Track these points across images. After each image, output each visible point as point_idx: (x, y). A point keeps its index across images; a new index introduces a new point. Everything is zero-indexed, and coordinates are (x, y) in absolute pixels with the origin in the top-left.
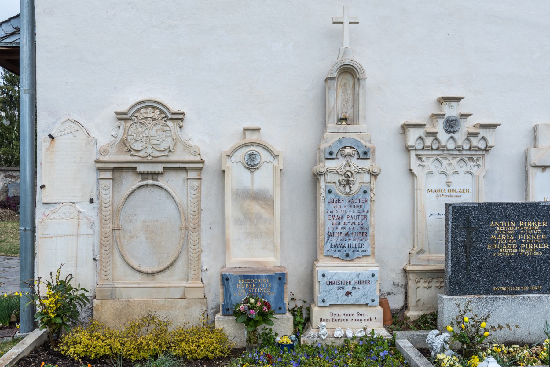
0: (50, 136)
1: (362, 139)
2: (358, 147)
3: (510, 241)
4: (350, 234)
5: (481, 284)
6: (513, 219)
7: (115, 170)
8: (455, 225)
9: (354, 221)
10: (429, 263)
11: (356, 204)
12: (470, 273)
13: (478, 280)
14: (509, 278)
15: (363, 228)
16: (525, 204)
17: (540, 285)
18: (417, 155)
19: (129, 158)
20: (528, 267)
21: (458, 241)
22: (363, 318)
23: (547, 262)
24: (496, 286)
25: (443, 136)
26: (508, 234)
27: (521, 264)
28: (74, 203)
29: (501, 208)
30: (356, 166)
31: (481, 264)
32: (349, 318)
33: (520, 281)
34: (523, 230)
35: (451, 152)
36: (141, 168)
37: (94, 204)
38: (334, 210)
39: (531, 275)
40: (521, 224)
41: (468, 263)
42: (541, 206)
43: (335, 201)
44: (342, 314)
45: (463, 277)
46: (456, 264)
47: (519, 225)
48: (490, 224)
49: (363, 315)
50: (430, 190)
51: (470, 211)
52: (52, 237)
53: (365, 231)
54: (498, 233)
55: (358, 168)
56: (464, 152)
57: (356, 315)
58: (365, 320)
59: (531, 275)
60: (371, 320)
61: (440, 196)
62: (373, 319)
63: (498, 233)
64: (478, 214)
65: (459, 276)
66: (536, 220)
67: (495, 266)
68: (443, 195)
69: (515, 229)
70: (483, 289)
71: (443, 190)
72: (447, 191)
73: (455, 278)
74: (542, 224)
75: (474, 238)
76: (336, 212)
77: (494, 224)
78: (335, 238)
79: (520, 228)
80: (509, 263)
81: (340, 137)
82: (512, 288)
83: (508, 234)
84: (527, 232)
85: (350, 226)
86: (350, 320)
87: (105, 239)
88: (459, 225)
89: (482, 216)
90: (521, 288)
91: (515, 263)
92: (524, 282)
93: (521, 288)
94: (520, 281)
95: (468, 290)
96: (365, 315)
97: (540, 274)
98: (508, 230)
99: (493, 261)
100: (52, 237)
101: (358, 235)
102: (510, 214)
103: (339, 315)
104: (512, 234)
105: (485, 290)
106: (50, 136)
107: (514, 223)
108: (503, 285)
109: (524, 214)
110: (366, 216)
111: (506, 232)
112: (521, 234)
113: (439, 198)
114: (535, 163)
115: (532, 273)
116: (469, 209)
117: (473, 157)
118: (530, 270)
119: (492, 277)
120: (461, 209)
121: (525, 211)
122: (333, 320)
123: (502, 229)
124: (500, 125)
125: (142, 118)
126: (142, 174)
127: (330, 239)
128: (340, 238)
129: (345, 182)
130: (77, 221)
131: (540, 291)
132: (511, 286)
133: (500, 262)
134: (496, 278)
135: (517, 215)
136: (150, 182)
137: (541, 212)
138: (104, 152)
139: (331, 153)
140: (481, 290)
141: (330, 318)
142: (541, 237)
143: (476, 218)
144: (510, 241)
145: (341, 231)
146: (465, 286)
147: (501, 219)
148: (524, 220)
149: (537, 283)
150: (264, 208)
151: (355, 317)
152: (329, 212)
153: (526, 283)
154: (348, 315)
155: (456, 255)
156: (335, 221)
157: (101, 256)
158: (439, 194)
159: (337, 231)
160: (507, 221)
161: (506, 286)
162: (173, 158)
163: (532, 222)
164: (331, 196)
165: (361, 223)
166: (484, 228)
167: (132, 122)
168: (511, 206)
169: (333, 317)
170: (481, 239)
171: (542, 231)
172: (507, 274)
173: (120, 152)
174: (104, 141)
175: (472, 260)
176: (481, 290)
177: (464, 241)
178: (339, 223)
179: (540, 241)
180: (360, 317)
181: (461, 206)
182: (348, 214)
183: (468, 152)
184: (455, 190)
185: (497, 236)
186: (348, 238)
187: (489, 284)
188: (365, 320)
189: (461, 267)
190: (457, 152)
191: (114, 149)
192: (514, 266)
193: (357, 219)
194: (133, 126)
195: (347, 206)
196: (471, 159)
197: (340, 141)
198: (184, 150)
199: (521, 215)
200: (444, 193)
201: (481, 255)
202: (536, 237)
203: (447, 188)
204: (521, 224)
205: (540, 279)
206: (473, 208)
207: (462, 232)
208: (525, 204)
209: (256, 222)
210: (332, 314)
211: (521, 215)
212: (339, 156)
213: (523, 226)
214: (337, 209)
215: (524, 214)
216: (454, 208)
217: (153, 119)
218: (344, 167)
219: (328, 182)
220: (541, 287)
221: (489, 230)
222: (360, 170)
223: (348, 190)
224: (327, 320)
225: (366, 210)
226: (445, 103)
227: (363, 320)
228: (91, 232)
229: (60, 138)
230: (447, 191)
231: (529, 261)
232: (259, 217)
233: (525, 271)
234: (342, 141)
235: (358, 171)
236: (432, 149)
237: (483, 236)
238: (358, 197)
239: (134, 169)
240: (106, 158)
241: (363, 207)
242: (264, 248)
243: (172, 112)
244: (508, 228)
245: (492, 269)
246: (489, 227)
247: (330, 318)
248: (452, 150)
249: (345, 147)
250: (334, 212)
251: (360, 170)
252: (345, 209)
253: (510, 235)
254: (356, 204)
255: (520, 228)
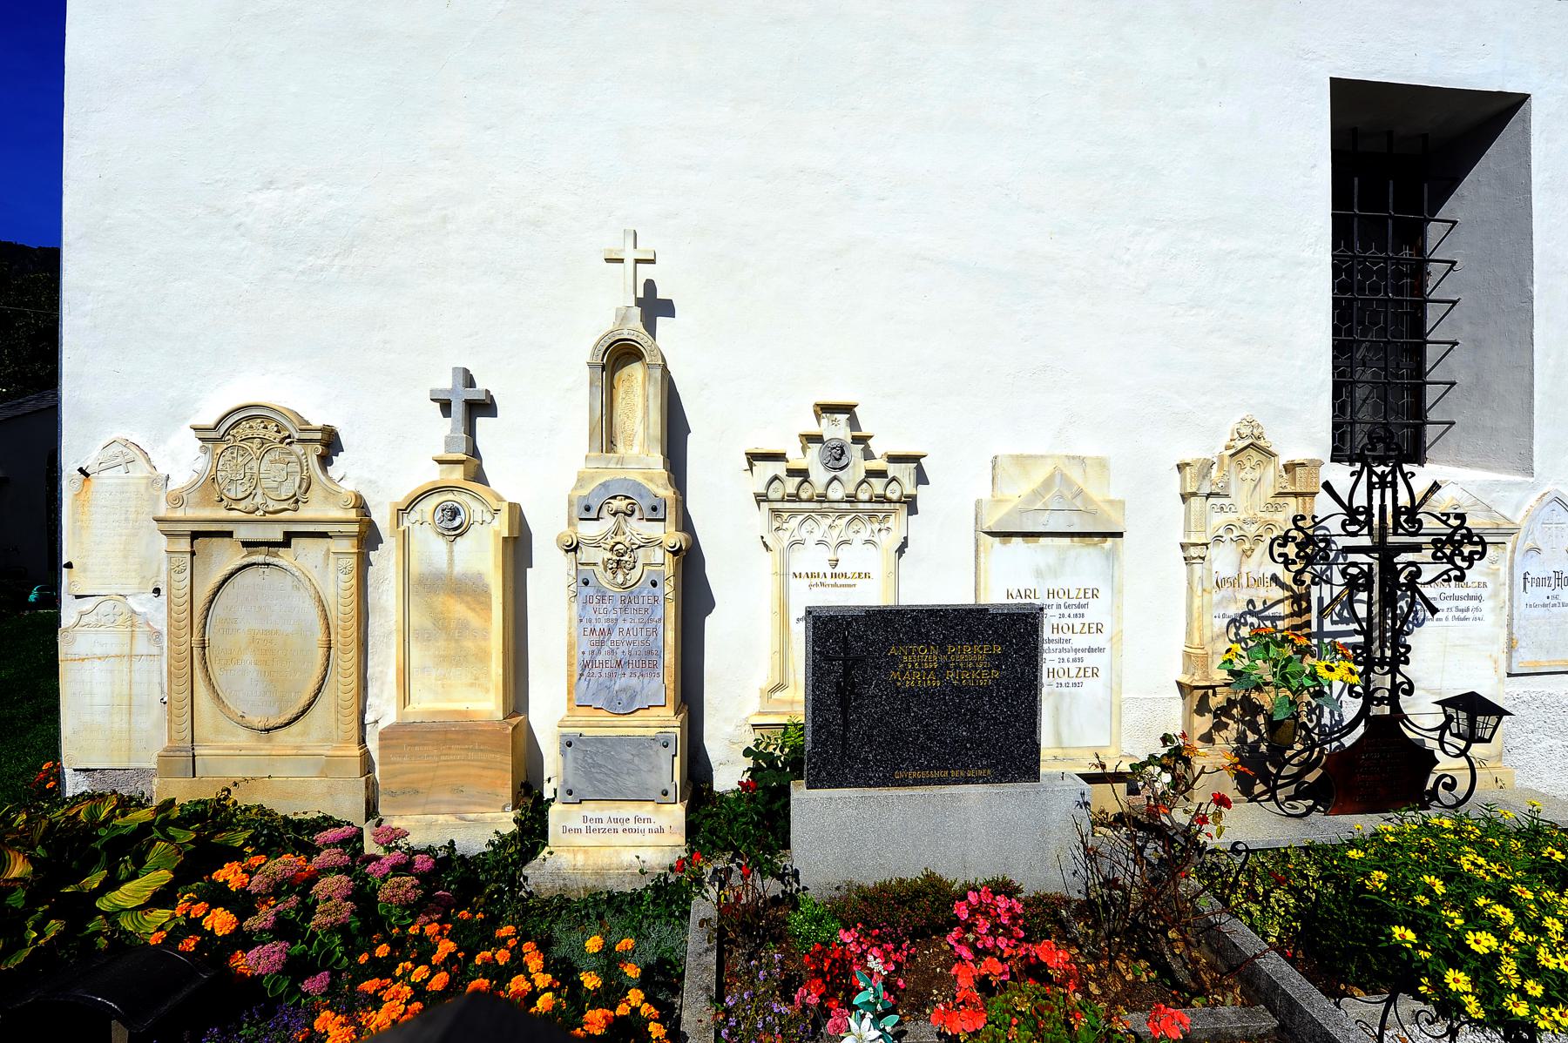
0: (81, 470)
1: (651, 480)
2: (641, 496)
3: (929, 682)
4: (625, 663)
5: (872, 766)
6: (935, 640)
7: (195, 535)
8: (819, 653)
9: (632, 638)
10: (792, 708)
11: (637, 606)
12: (850, 745)
13: (866, 758)
14: (925, 754)
15: (650, 652)
16: (959, 612)
17: (987, 767)
18: (773, 510)
19: (222, 514)
20: (964, 733)
21: (825, 683)
22: (647, 826)
23: (1001, 723)
24: (900, 769)
25: (819, 476)
26: (924, 670)
27: (950, 727)
28: (124, 596)
29: (910, 618)
30: (635, 533)
31: (870, 728)
32: (619, 827)
33: (947, 760)
34: (954, 662)
35: (836, 505)
36: (243, 533)
37: (163, 597)
38: (594, 617)
39: (970, 749)
40: (951, 649)
41: (846, 724)
42: (990, 614)
43: (595, 601)
44: (605, 820)
45: (835, 754)
46: (821, 727)
47: (946, 653)
48: (889, 650)
49: (646, 821)
50: (797, 574)
51: (849, 624)
52: (83, 660)
53: (654, 658)
54: (905, 668)
55: (639, 537)
56: (861, 506)
57: (632, 820)
58: (650, 831)
59: (970, 749)
60: (661, 830)
61: (817, 585)
62: (667, 829)
63: (905, 668)
64: (865, 631)
65: (827, 752)
66: (980, 642)
67: (899, 731)
68: (822, 584)
69: (938, 659)
70: (875, 775)
71: (821, 575)
72: (829, 575)
73: (820, 754)
74: (992, 650)
75: (857, 678)
76: (598, 620)
77: (897, 649)
78: (595, 670)
79: (949, 658)
80: (927, 725)
81: (607, 478)
82: (933, 773)
83: (924, 670)
84: (961, 665)
85: (625, 648)
86: (620, 831)
87: (177, 664)
88: (828, 652)
89: (872, 634)
90: (949, 774)
91: (938, 726)
92: (956, 762)
93: (949, 774)
94: (947, 760)
95: (846, 779)
96: (649, 820)
97: (988, 745)
98: (924, 662)
99: (895, 722)
100: (83, 660)
101: (641, 666)
102: (929, 631)
103: (600, 820)
104: (933, 669)
105: (879, 778)
106: (81, 470)
107: (936, 649)
108: (914, 768)
109: (955, 630)
110: (655, 630)
111: (920, 665)
112: (951, 670)
113: (814, 588)
114: (989, 527)
115: (972, 745)
116: (846, 621)
117: (878, 514)
118: (969, 740)
119: (893, 753)
120: (831, 621)
121: (957, 625)
122: (588, 830)
123: (913, 659)
124: (925, 456)
125: (244, 437)
126: (246, 544)
127: (586, 673)
128: (606, 671)
129: (615, 565)
130: (129, 629)
131: (988, 780)
132: (931, 769)
133: (908, 724)
134: (902, 755)
135: (942, 633)
136: (259, 558)
137: (990, 626)
138: (178, 500)
139: (588, 509)
140: (871, 779)
141: (583, 827)
142: (990, 674)
143: (861, 637)
144: (929, 682)
145: (607, 657)
146: (839, 769)
147: (911, 641)
148: (957, 642)
149: (981, 764)
150: (473, 610)
151: (631, 825)
152: (584, 620)
153: (960, 764)
154: (616, 821)
155: (820, 710)
156: (595, 638)
157: (170, 698)
158: (814, 581)
159: (599, 658)
160: (923, 644)
161: (920, 770)
162: (305, 512)
163: (972, 646)
164: (589, 590)
165: (645, 642)
166: (877, 658)
167: (225, 446)
168: (931, 615)
169: (588, 824)
170: (871, 679)
171: (991, 663)
172: (923, 746)
173: (204, 502)
174: (182, 478)
175: (854, 719)
176: (871, 779)
177: (838, 683)
178: (602, 643)
179: (987, 683)
180: (641, 826)
181: (831, 616)
182: (620, 624)
183: (868, 506)
184: (845, 575)
185: (903, 674)
186: (620, 671)
187: (887, 767)
188: (650, 831)
189: (831, 734)
190: (848, 506)
191: (194, 497)
192: (937, 730)
193: (639, 635)
194: (227, 453)
195: (619, 610)
196: (872, 515)
197: (604, 485)
198: (326, 498)
199: (951, 633)
200: (823, 580)
201: (871, 711)
202: (979, 675)
203: (829, 571)
204: (951, 649)
205: (987, 755)
206: (856, 618)
207: (833, 665)
208: (959, 612)
209: (457, 635)
210: (585, 819)
211: (951, 633)
212: (604, 513)
213: (953, 653)
214: (600, 616)
215: (955, 630)
216: (817, 619)
217: (263, 441)
218: (613, 535)
219: (582, 564)
220: (989, 772)
221: (888, 663)
222: (643, 540)
223: (620, 579)
224: (578, 831)
225: (656, 619)
226: (824, 415)
227: (647, 831)
228: (155, 650)
229: (103, 474)
230: (829, 575)
231: (966, 722)
232: (464, 626)
233: (957, 742)
234: (609, 486)
235: (638, 542)
236: (801, 501)
237: (874, 674)
238: (640, 592)
239: (229, 534)
240: (179, 514)
241: (650, 611)
242: (472, 685)
243: (213, 427)
244: (924, 658)
245: (892, 736)
246: (886, 656)
247: (583, 827)
248: (838, 502)
249: (614, 497)
250: (594, 621)
251: (643, 540)
252: (614, 616)
253: (928, 671)
254: (637, 606)
255: (949, 658)
